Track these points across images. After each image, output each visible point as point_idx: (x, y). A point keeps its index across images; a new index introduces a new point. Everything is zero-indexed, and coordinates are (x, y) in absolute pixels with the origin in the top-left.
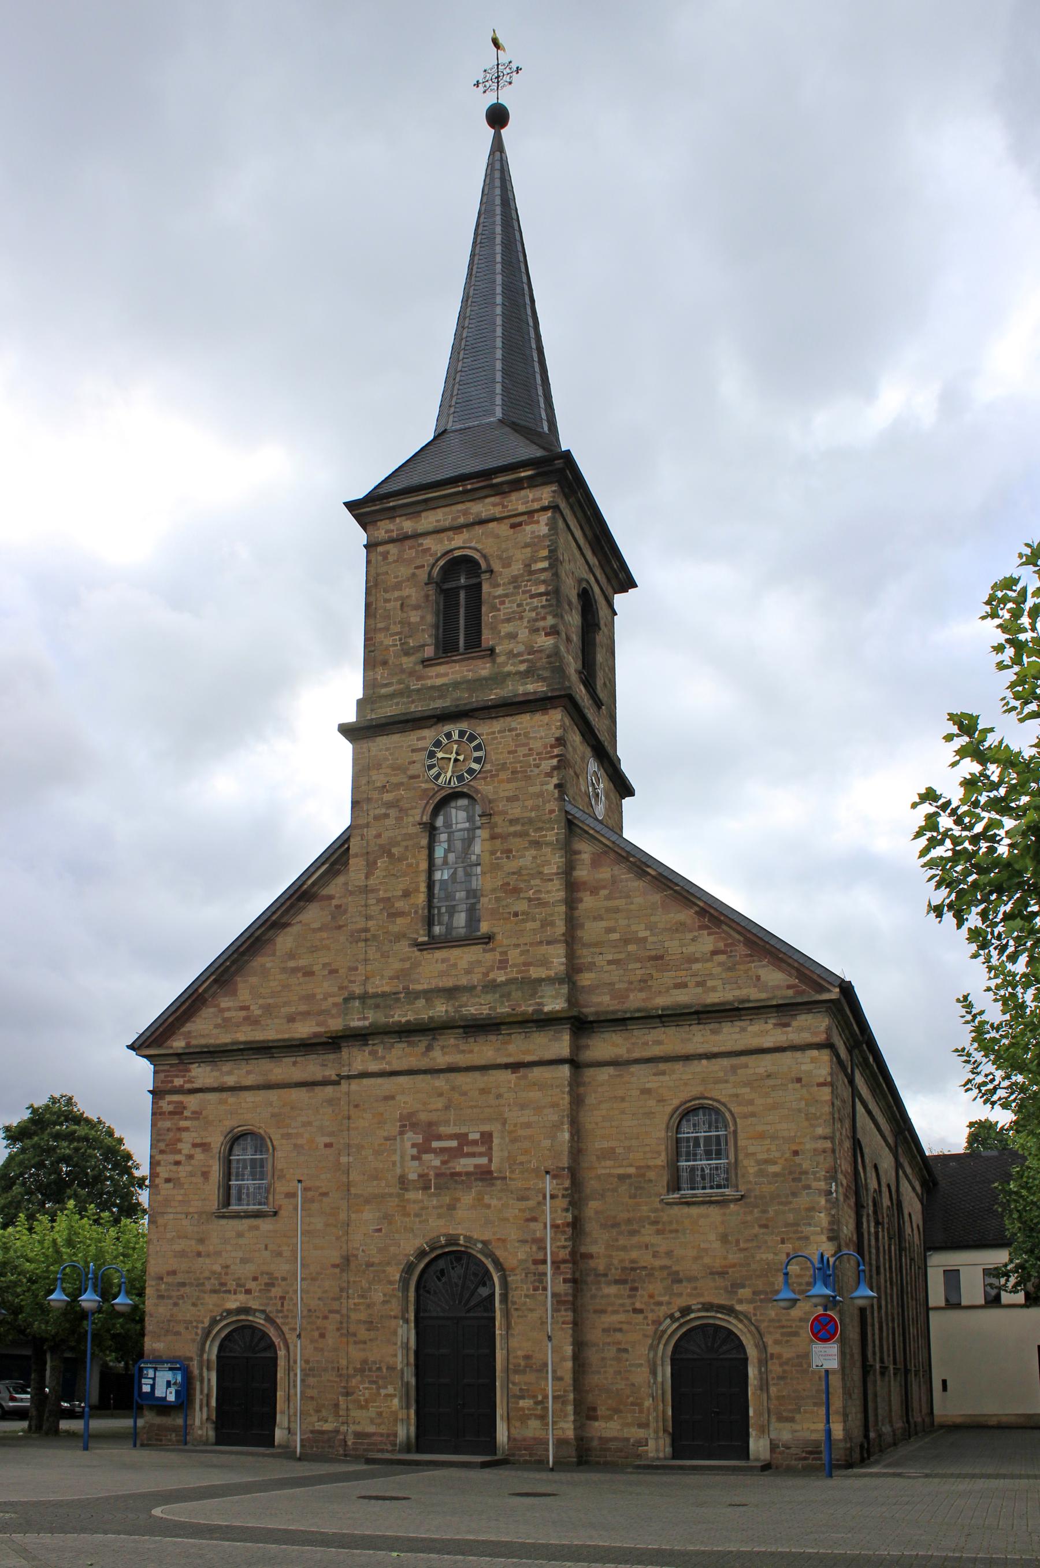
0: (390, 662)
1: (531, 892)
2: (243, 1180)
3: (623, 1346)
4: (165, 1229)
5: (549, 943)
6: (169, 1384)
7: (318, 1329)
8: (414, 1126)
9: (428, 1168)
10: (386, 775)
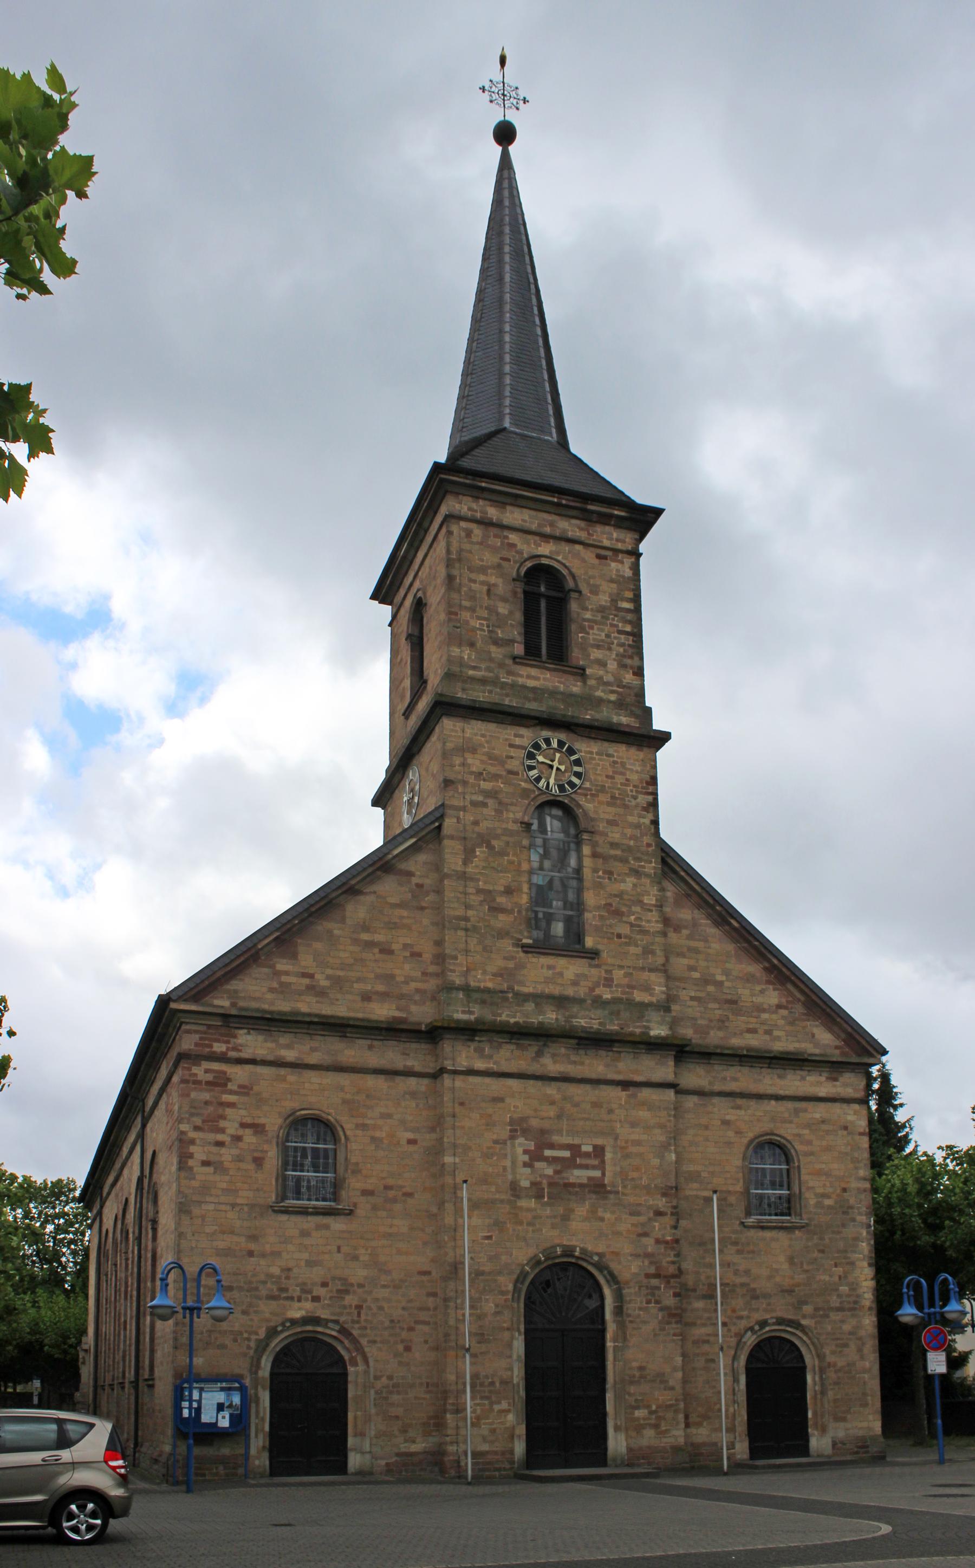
0: (478, 645)
1: (632, 918)
2: (302, 1171)
3: (711, 1357)
4: (203, 1220)
5: (650, 970)
6: (220, 1407)
7: (402, 1341)
8: (526, 1132)
9: (540, 1176)
10: (482, 762)
